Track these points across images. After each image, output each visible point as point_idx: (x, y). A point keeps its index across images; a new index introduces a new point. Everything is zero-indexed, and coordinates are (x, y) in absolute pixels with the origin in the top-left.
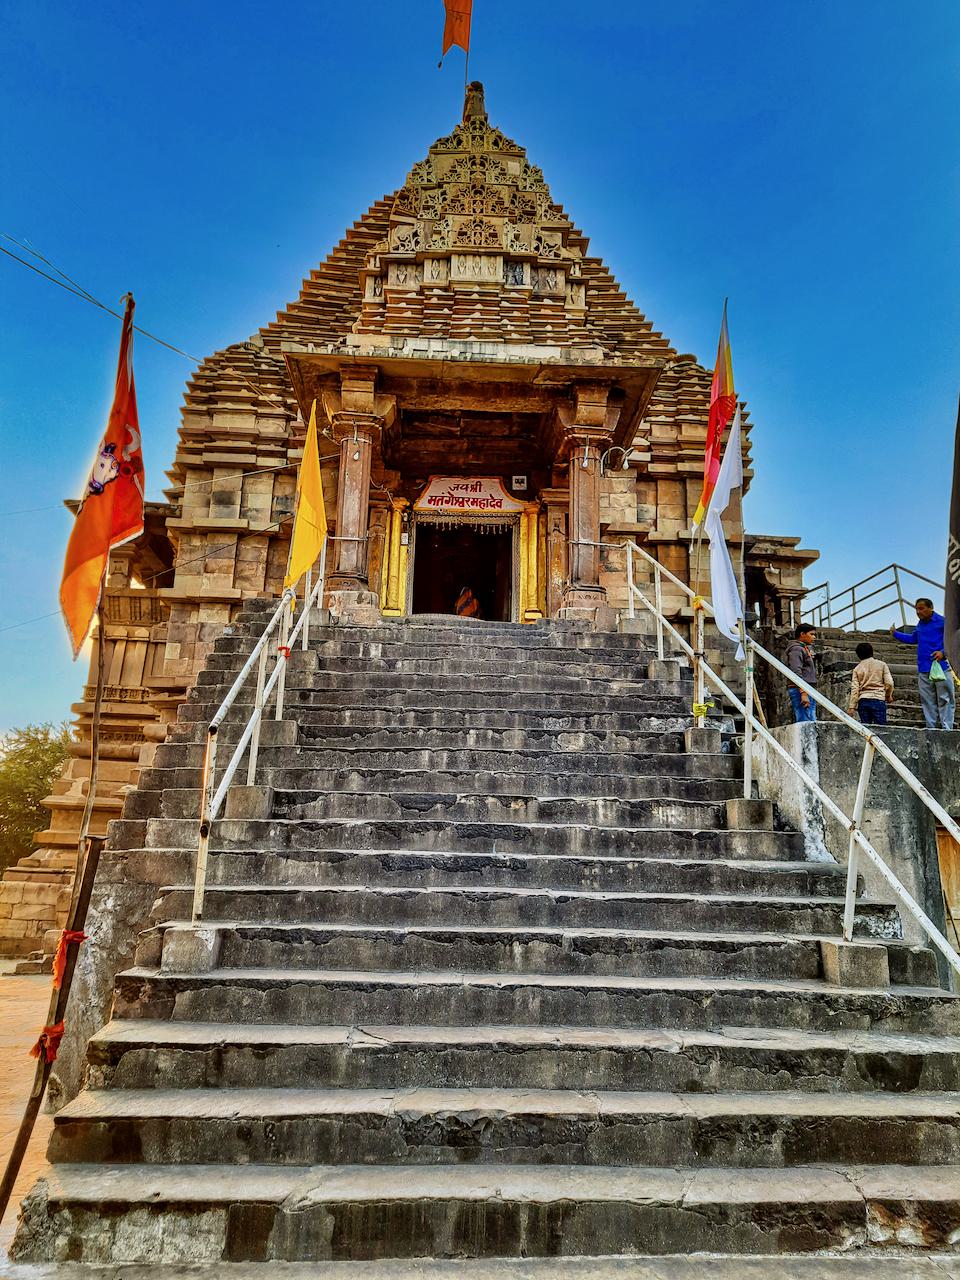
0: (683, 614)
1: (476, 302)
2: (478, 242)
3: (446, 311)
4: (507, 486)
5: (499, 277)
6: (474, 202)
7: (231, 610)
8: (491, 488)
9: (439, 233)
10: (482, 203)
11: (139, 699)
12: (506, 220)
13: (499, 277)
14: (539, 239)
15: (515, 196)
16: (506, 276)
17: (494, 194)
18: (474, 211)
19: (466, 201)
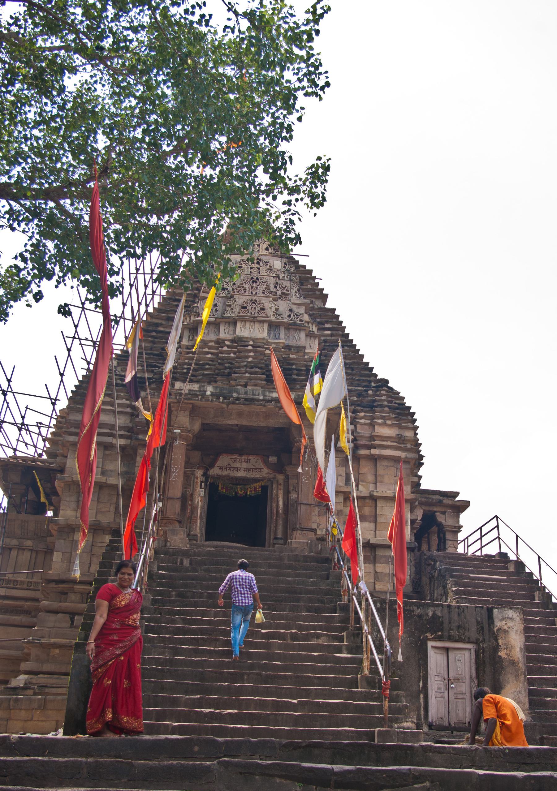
0: (371, 542)
1: (250, 351)
2: (253, 313)
3: (232, 355)
4: (266, 463)
5: (265, 334)
6: (252, 287)
7: (94, 533)
8: (255, 461)
9: (230, 306)
10: (257, 288)
11: (12, 586)
12: (271, 299)
13: (265, 334)
14: (291, 310)
15: (277, 283)
16: (269, 334)
17: (267, 263)
18: (252, 293)
19: (247, 286)
